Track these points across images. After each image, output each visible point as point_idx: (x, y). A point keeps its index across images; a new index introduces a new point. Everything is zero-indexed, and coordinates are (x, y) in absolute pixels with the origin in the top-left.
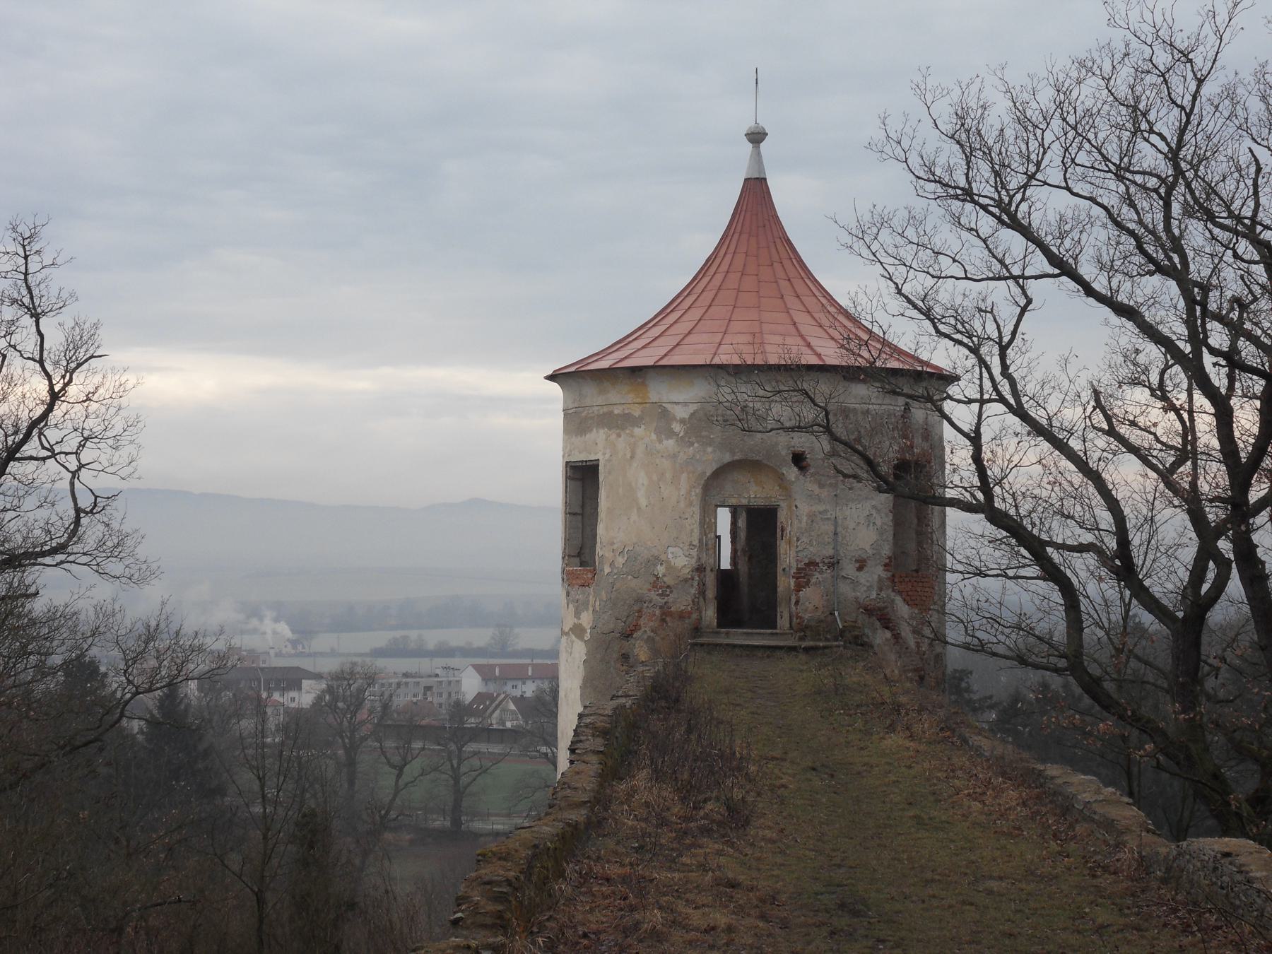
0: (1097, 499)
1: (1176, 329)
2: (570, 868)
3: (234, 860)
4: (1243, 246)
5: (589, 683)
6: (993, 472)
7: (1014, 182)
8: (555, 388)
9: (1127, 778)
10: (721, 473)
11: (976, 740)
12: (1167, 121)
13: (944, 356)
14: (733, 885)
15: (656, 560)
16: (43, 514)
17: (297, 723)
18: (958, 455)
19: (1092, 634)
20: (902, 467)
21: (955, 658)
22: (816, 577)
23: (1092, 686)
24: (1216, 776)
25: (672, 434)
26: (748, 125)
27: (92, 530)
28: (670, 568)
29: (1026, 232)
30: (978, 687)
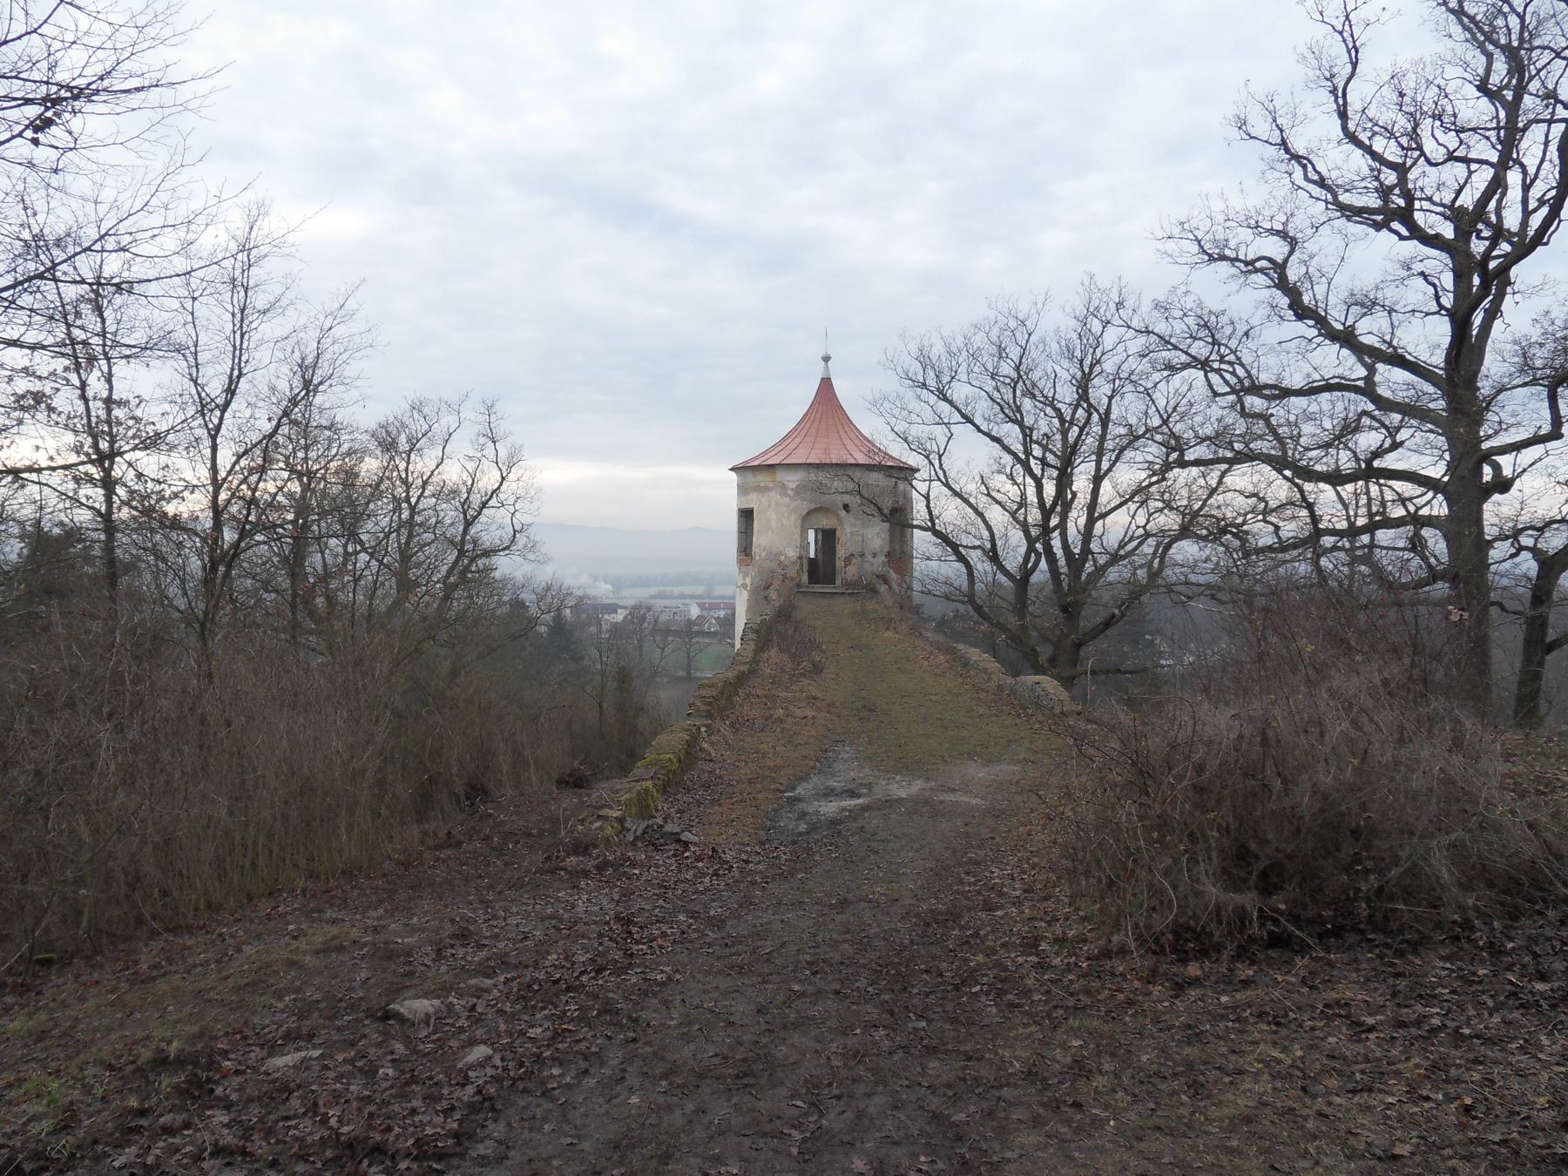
0: (982, 525)
1: (1018, 448)
2: (741, 691)
3: (589, 688)
4: (1049, 410)
5: (749, 609)
6: (935, 513)
7: (945, 379)
8: (733, 475)
9: (994, 651)
10: (810, 513)
11: (927, 634)
12: (1014, 353)
13: (913, 460)
14: (815, 698)
15: (780, 554)
16: (498, 533)
17: (616, 629)
18: (919, 507)
19: (979, 586)
20: (894, 511)
21: (917, 598)
23: (978, 609)
24: (1033, 650)
25: (787, 495)
26: (823, 353)
27: (521, 540)
29: (951, 403)
30: (927, 612)
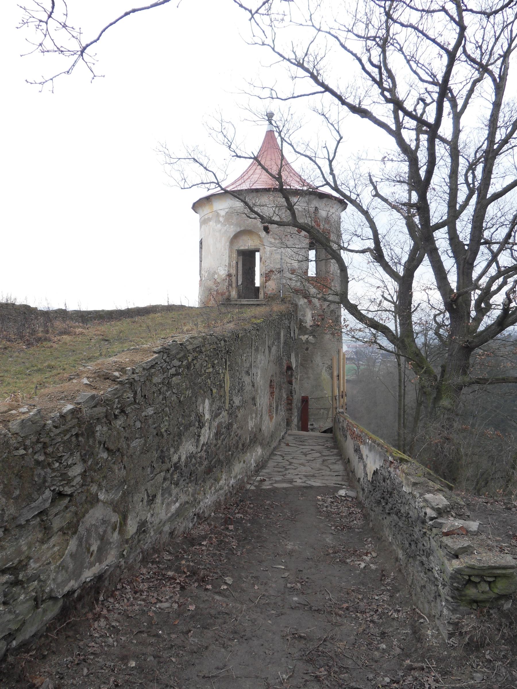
22: (273, 277)
25: (219, 222)
28: (219, 275)
